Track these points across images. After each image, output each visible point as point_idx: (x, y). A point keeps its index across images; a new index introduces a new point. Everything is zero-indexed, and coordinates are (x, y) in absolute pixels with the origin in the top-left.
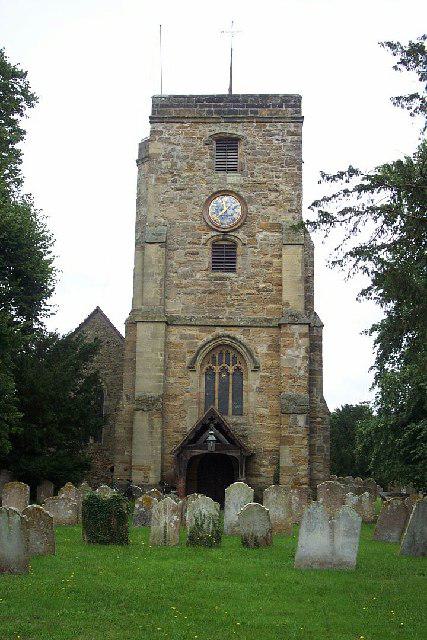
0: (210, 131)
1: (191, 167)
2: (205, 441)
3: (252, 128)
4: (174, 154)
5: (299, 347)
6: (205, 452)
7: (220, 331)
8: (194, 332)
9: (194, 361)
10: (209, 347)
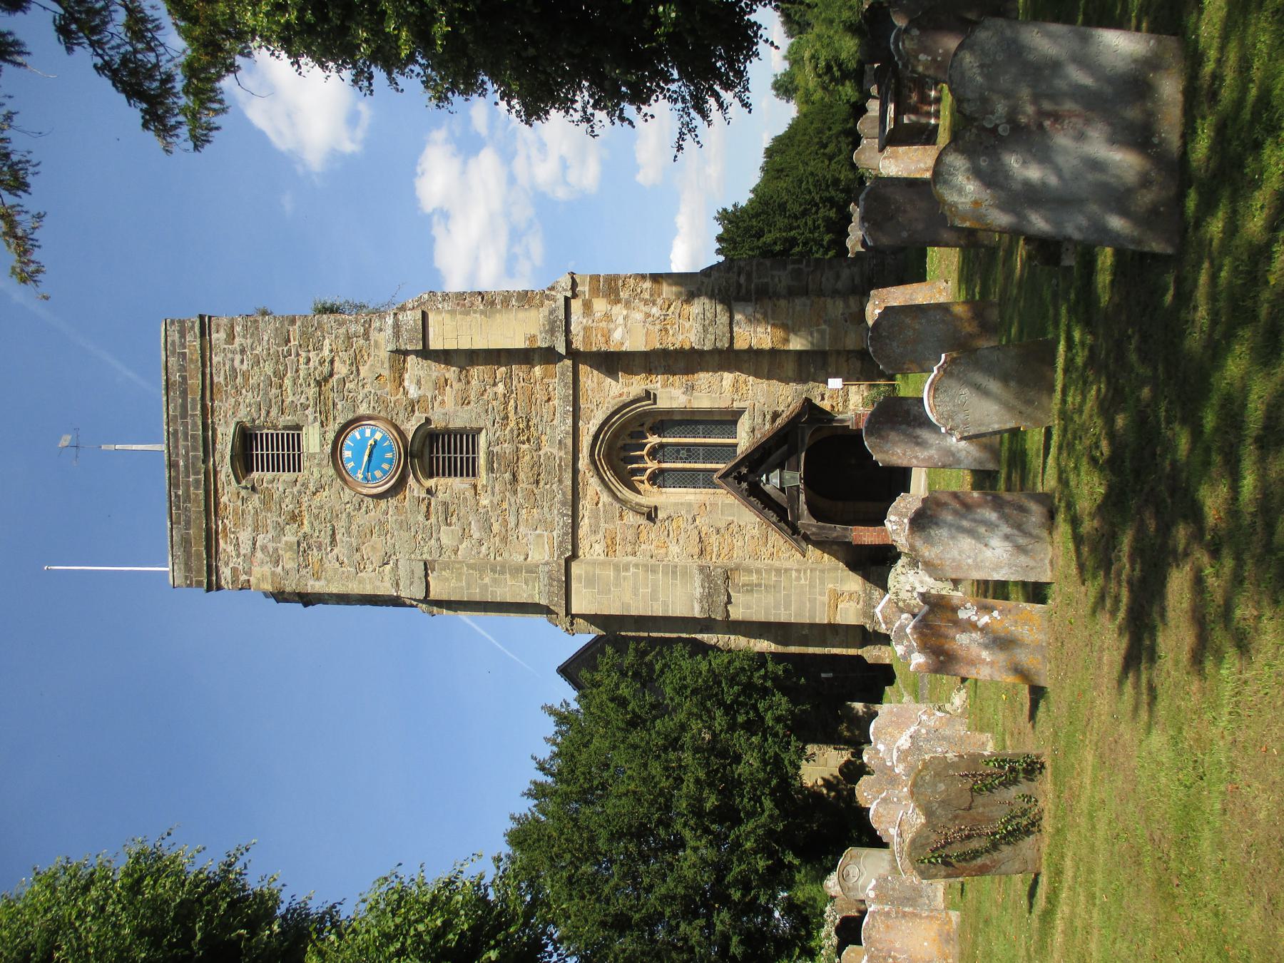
0: (229, 484)
1: (294, 518)
2: (782, 489)
3: (223, 406)
4: (271, 546)
5: (608, 317)
6: (802, 497)
7: (583, 463)
8: (586, 506)
9: (637, 510)
10: (609, 475)
